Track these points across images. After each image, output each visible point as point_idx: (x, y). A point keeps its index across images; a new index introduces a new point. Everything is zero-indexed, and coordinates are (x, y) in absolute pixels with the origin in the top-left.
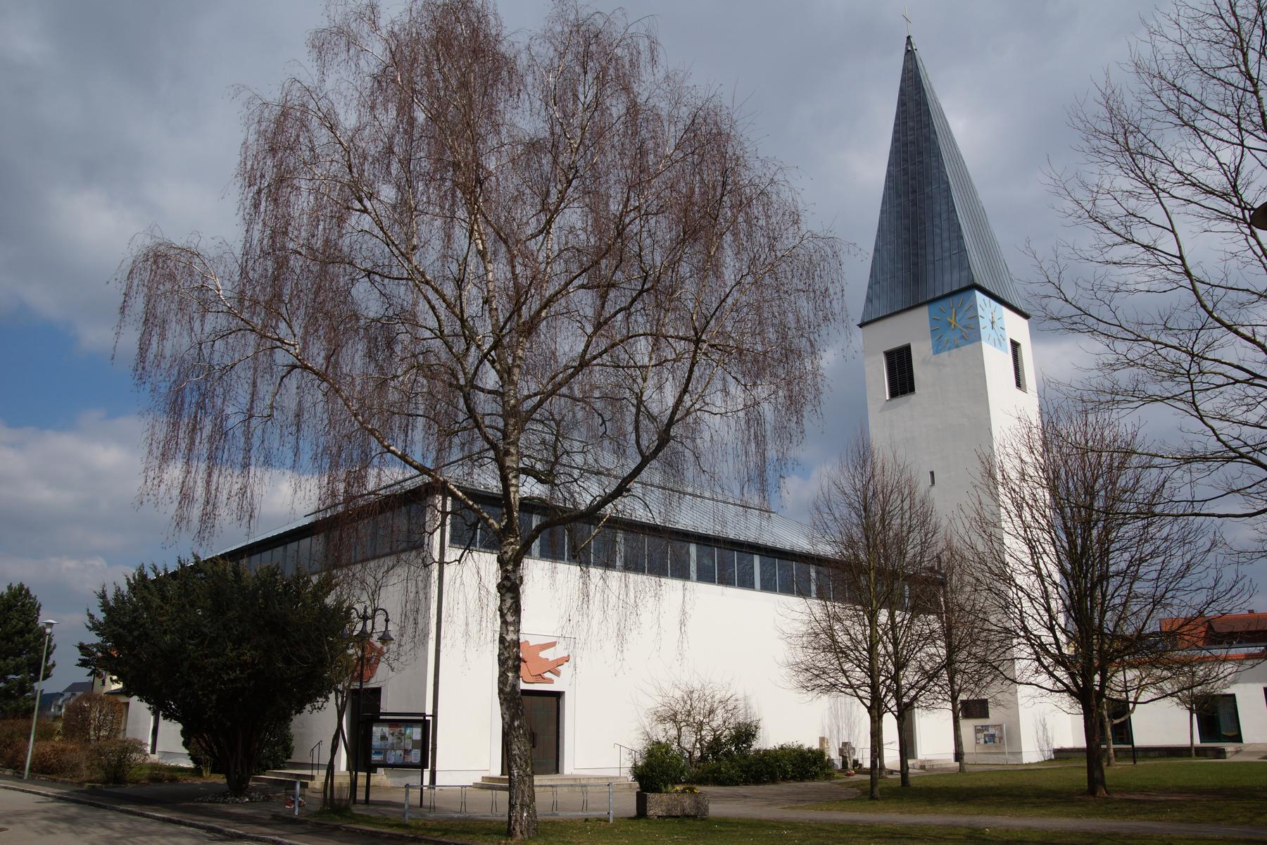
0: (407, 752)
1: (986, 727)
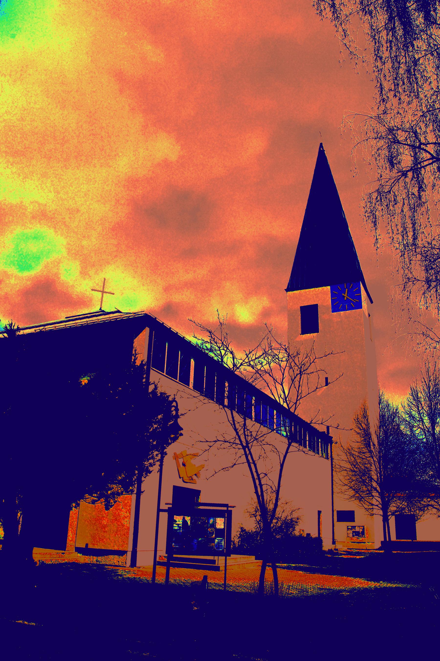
1: (354, 527)
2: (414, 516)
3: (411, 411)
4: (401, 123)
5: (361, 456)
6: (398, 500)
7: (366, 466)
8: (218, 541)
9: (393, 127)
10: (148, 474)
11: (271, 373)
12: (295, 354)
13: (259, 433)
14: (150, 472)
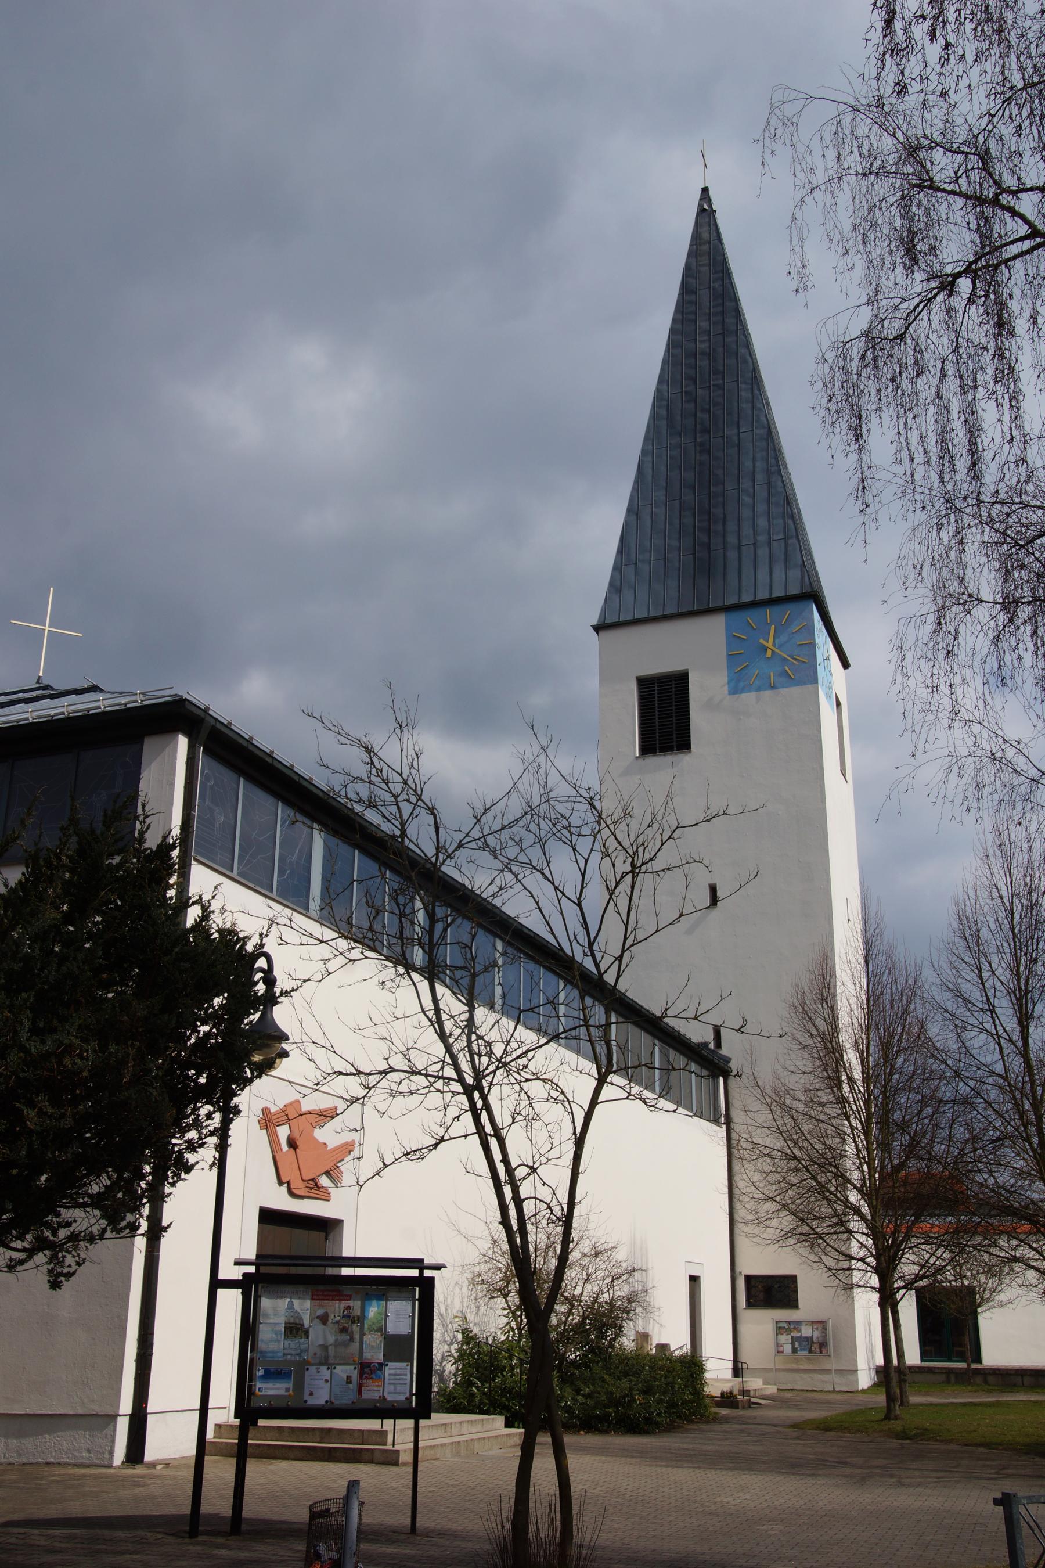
0: (368, 1370)
1: (796, 1325)
2: (971, 1291)
3: (960, 980)
4: (941, 126)
5: (813, 1113)
6: (923, 1243)
7: (829, 1142)
8: (392, 1372)
9: (918, 140)
10: (183, 1175)
11: (547, 872)
12: (618, 814)
13: (514, 1045)
14: (189, 1169)
